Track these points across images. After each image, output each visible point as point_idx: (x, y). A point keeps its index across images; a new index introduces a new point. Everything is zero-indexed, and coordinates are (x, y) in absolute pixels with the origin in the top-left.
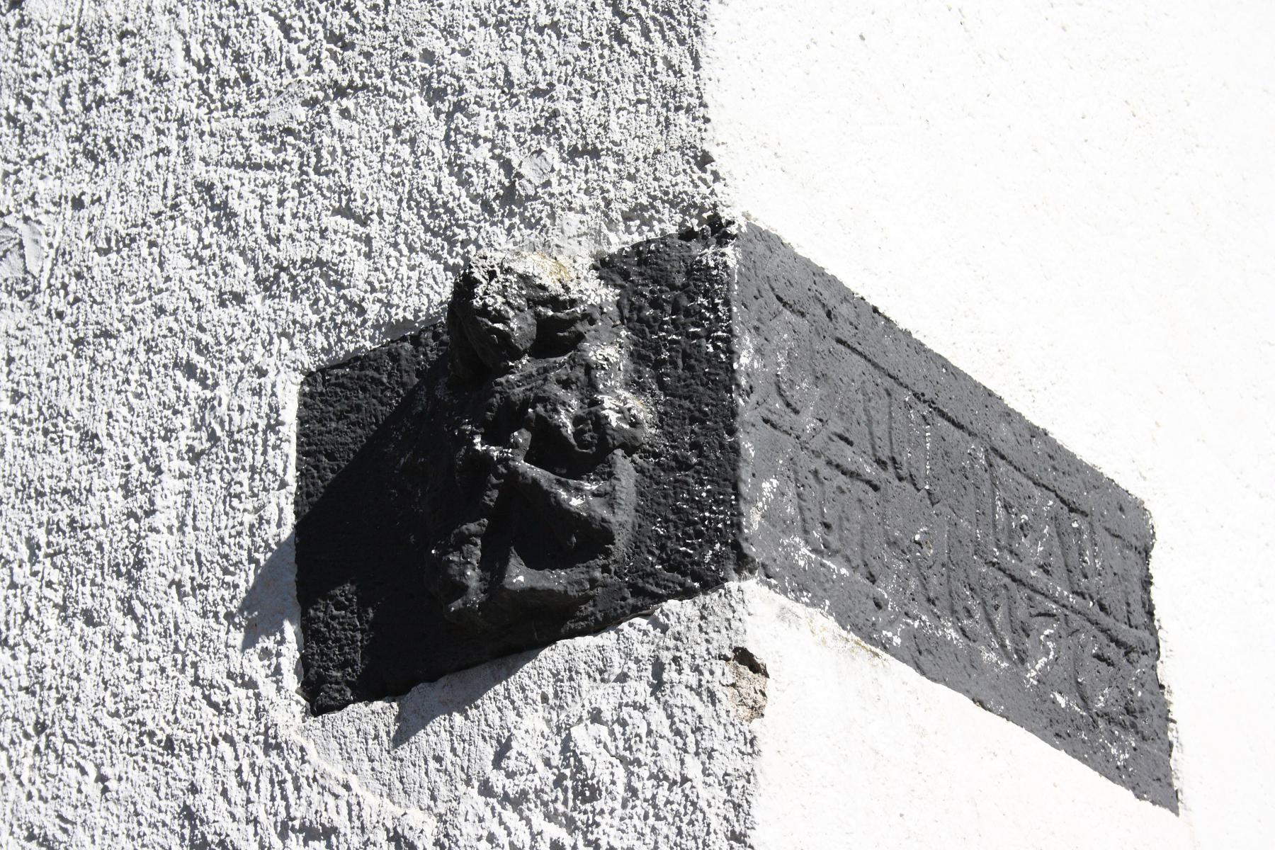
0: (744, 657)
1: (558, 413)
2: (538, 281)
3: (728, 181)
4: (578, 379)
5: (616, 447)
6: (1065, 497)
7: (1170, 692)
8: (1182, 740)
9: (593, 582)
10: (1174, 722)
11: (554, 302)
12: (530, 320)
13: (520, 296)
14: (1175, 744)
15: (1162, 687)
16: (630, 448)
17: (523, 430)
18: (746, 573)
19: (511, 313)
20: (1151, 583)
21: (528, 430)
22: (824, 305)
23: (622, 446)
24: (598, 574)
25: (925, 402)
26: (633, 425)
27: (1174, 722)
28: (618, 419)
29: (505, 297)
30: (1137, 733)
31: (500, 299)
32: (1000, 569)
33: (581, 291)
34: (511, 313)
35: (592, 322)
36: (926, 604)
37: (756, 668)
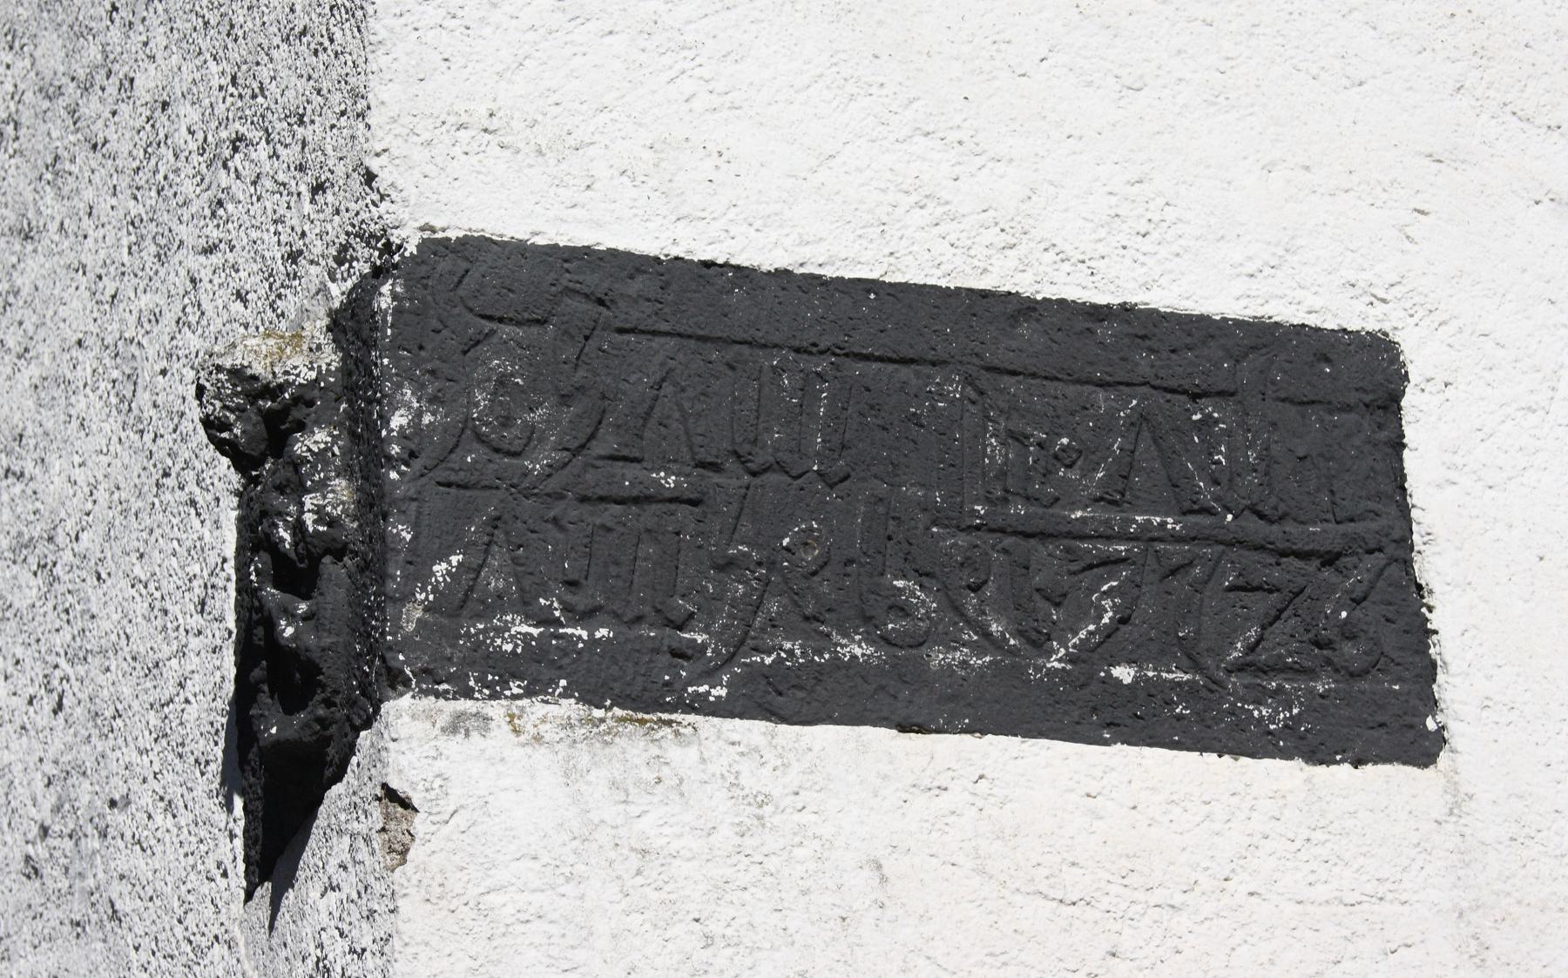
0: (391, 795)
1: (276, 526)
2: (249, 372)
3: (393, 197)
4: (288, 480)
5: (324, 555)
6: (1173, 383)
7: (1431, 592)
8: (1448, 658)
9: (319, 720)
10: (1436, 632)
11: (271, 391)
12: (255, 418)
13: (236, 394)
14: (1439, 663)
15: (1419, 587)
16: (339, 553)
17: (262, 553)
18: (400, 688)
19: (232, 417)
20: (1404, 446)
21: (265, 551)
22: (587, 296)
23: (327, 552)
24: (321, 712)
25: (822, 353)
26: (330, 525)
27: (1436, 632)
28: (315, 522)
29: (221, 400)
30: (1337, 671)
31: (218, 404)
32: (992, 531)
33: (286, 373)
34: (232, 417)
35: (310, 404)
36: (805, 625)
37: (406, 804)
